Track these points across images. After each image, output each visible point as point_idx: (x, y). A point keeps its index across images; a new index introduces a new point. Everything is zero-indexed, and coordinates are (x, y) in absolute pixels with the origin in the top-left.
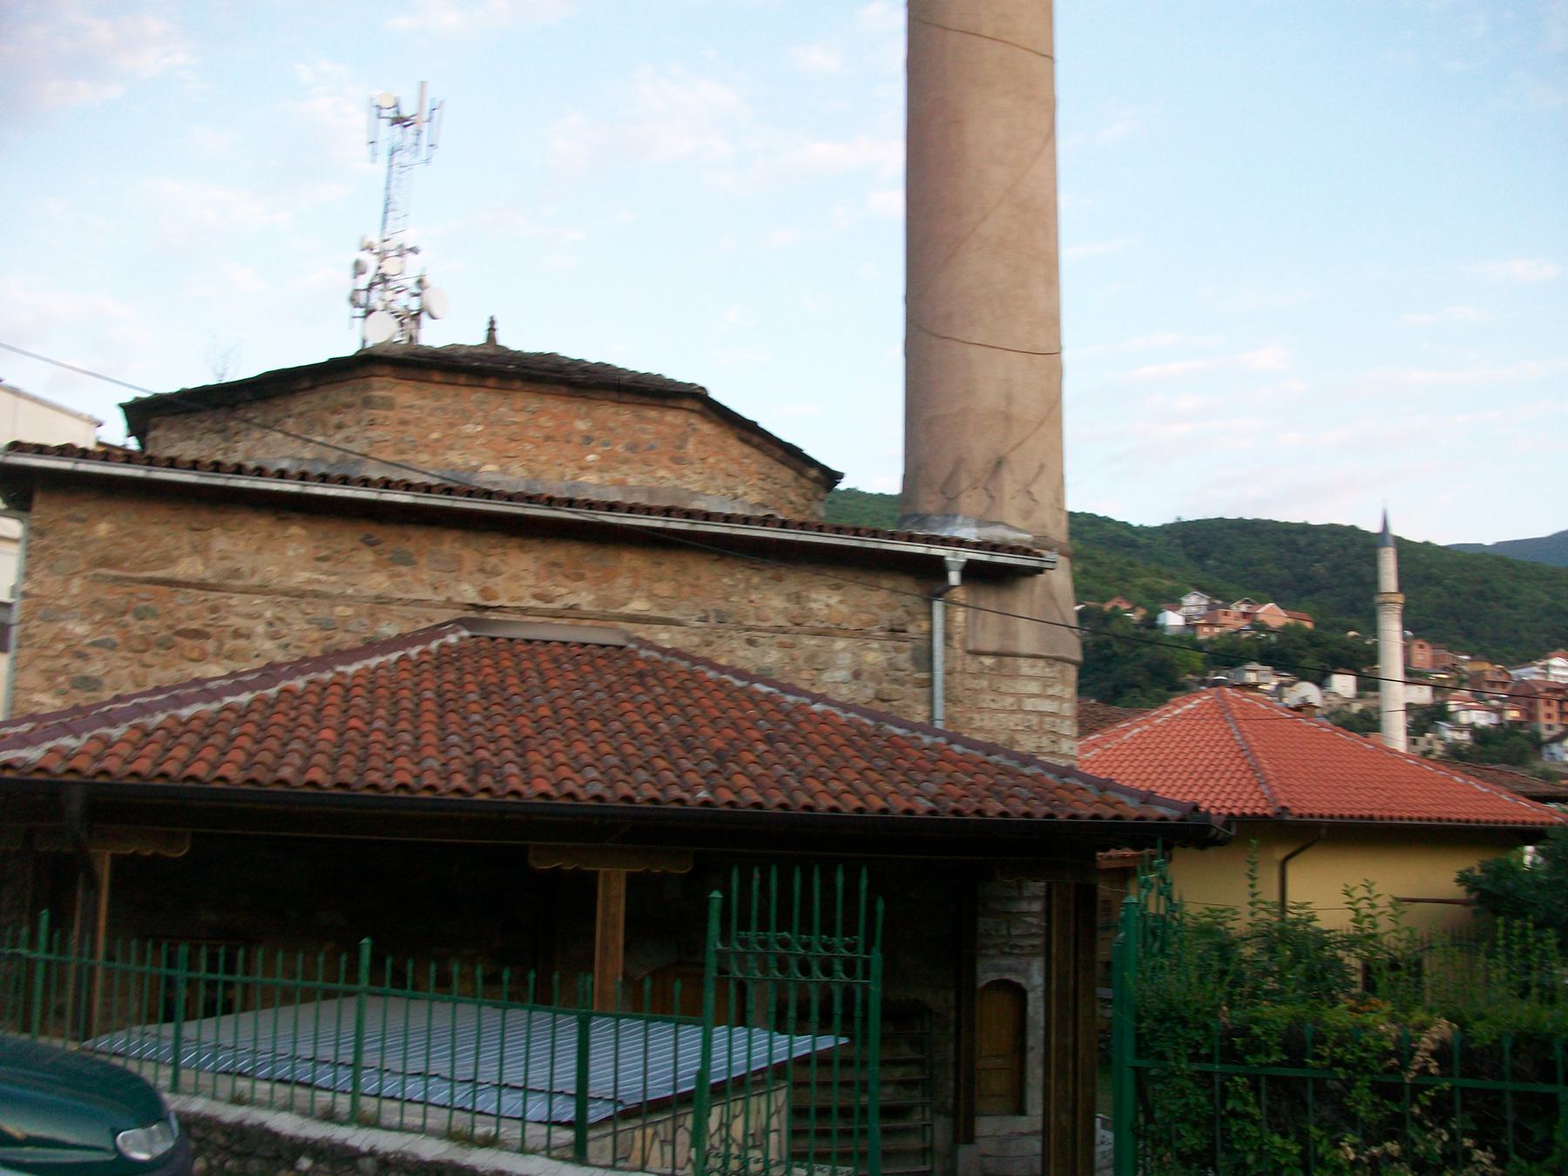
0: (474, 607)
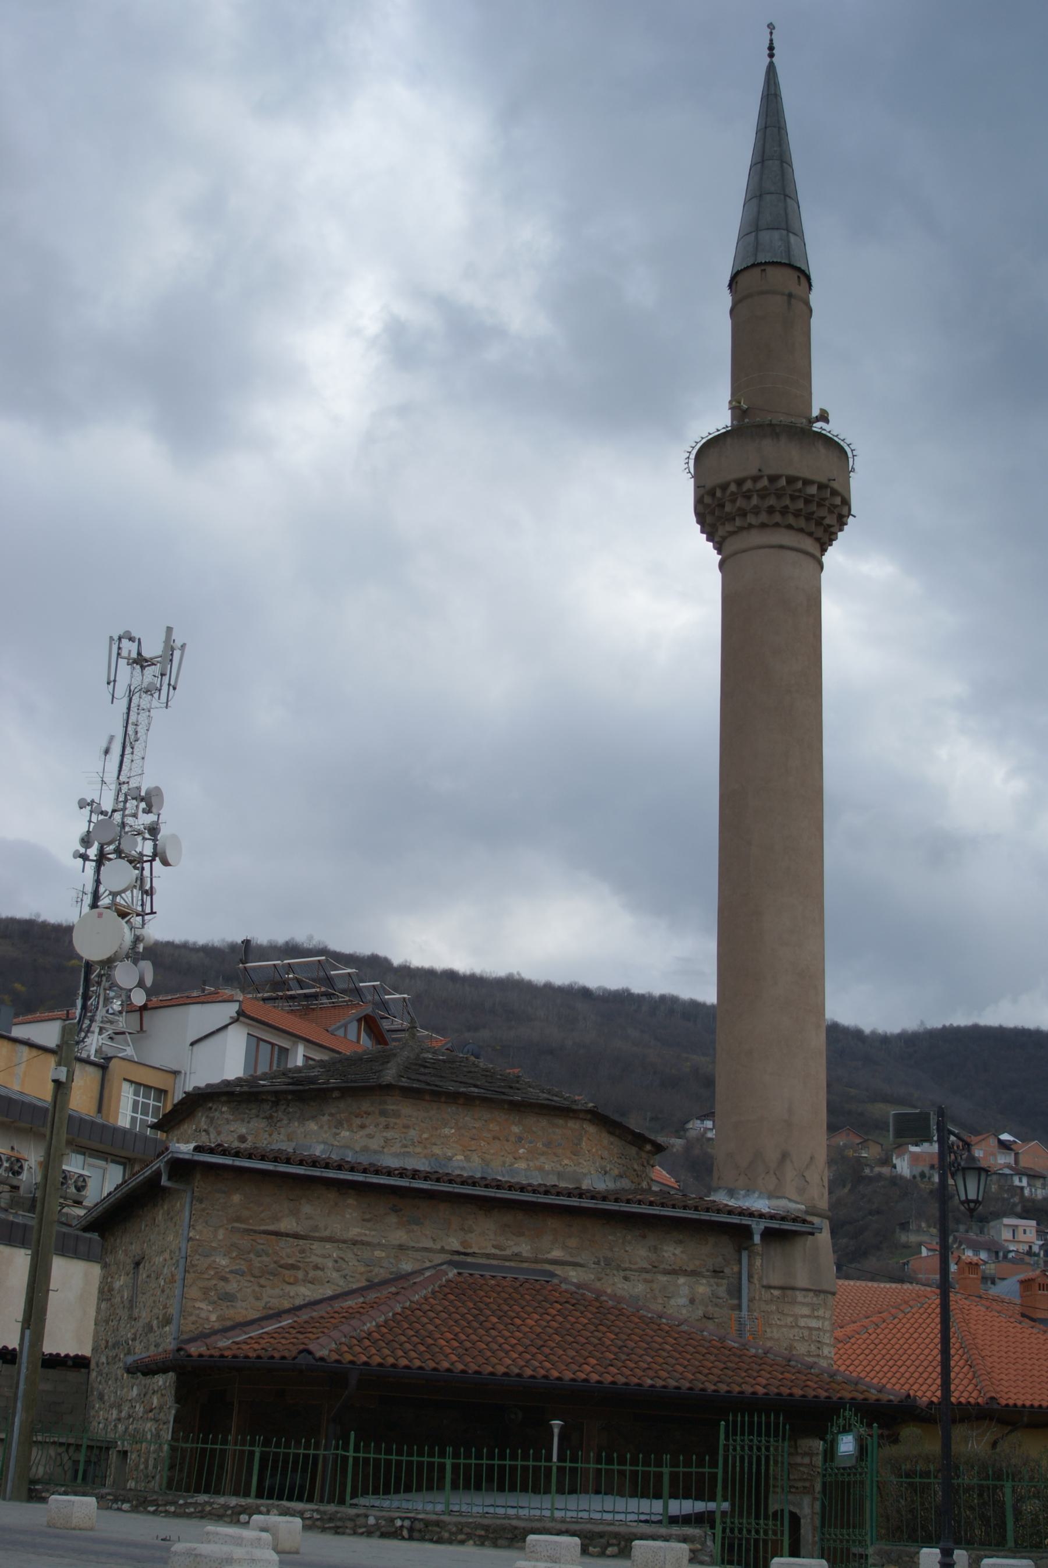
0: (458, 1253)
